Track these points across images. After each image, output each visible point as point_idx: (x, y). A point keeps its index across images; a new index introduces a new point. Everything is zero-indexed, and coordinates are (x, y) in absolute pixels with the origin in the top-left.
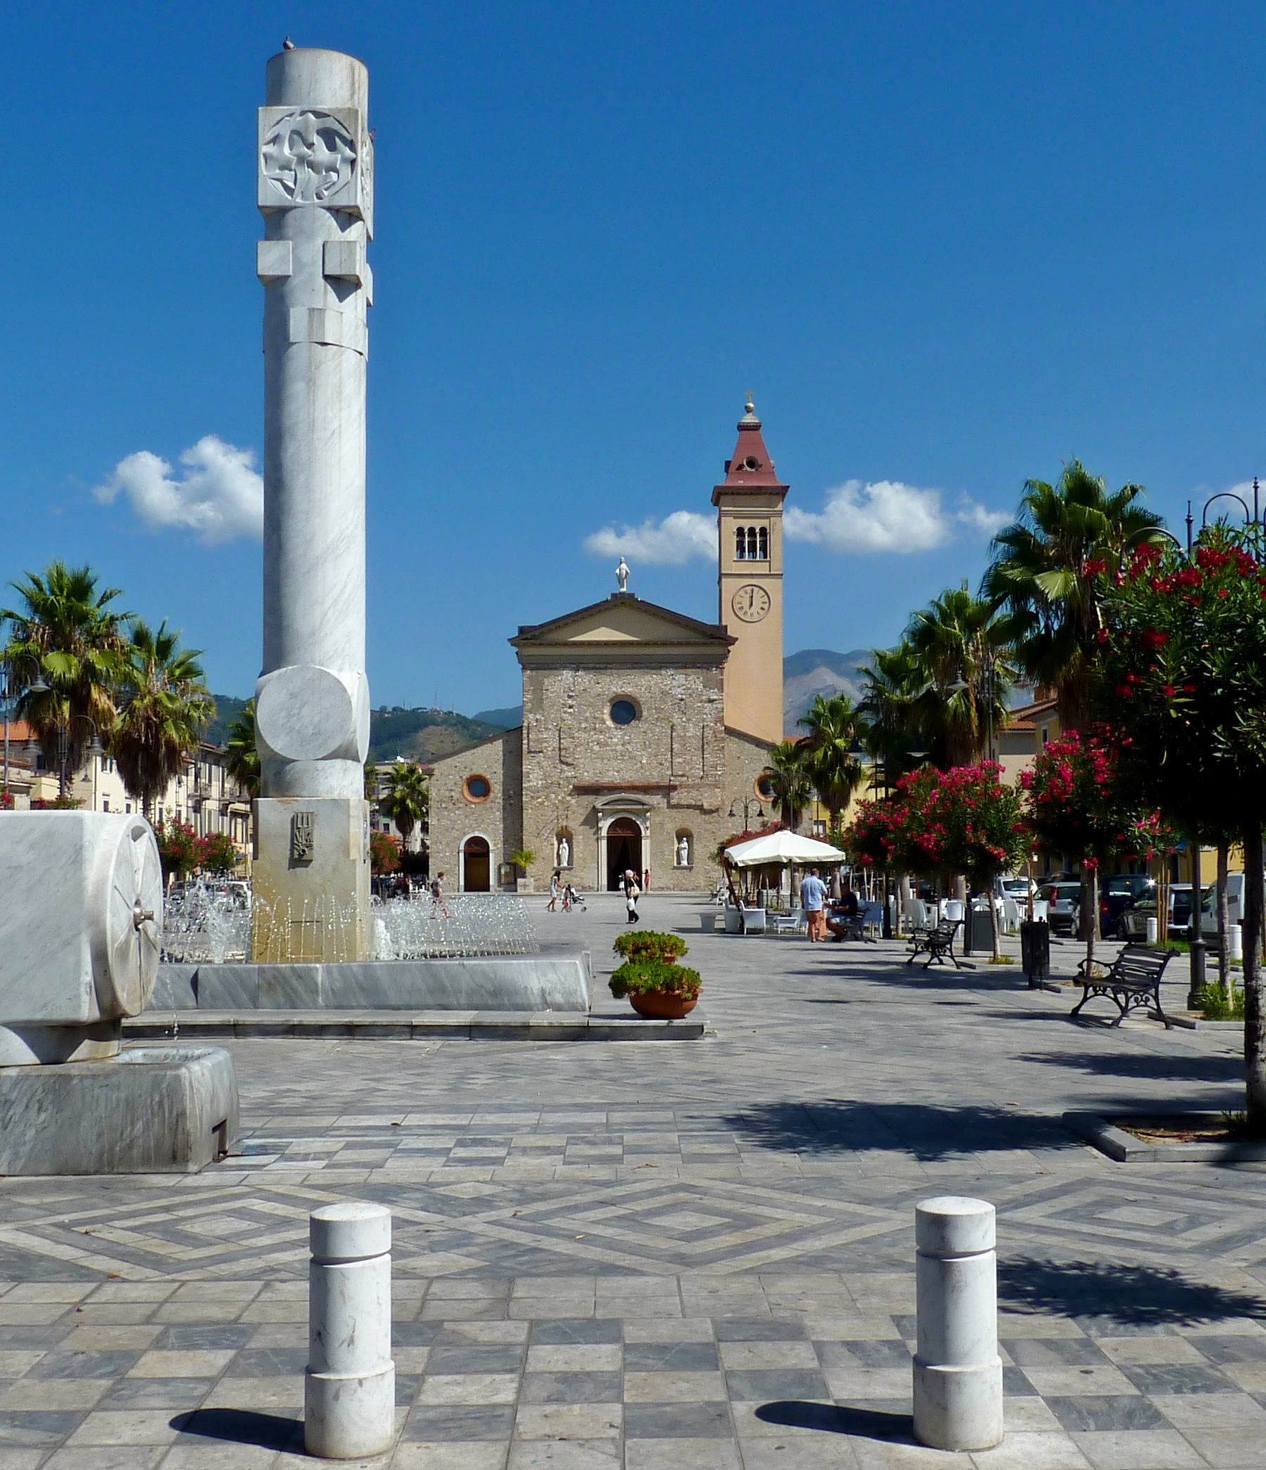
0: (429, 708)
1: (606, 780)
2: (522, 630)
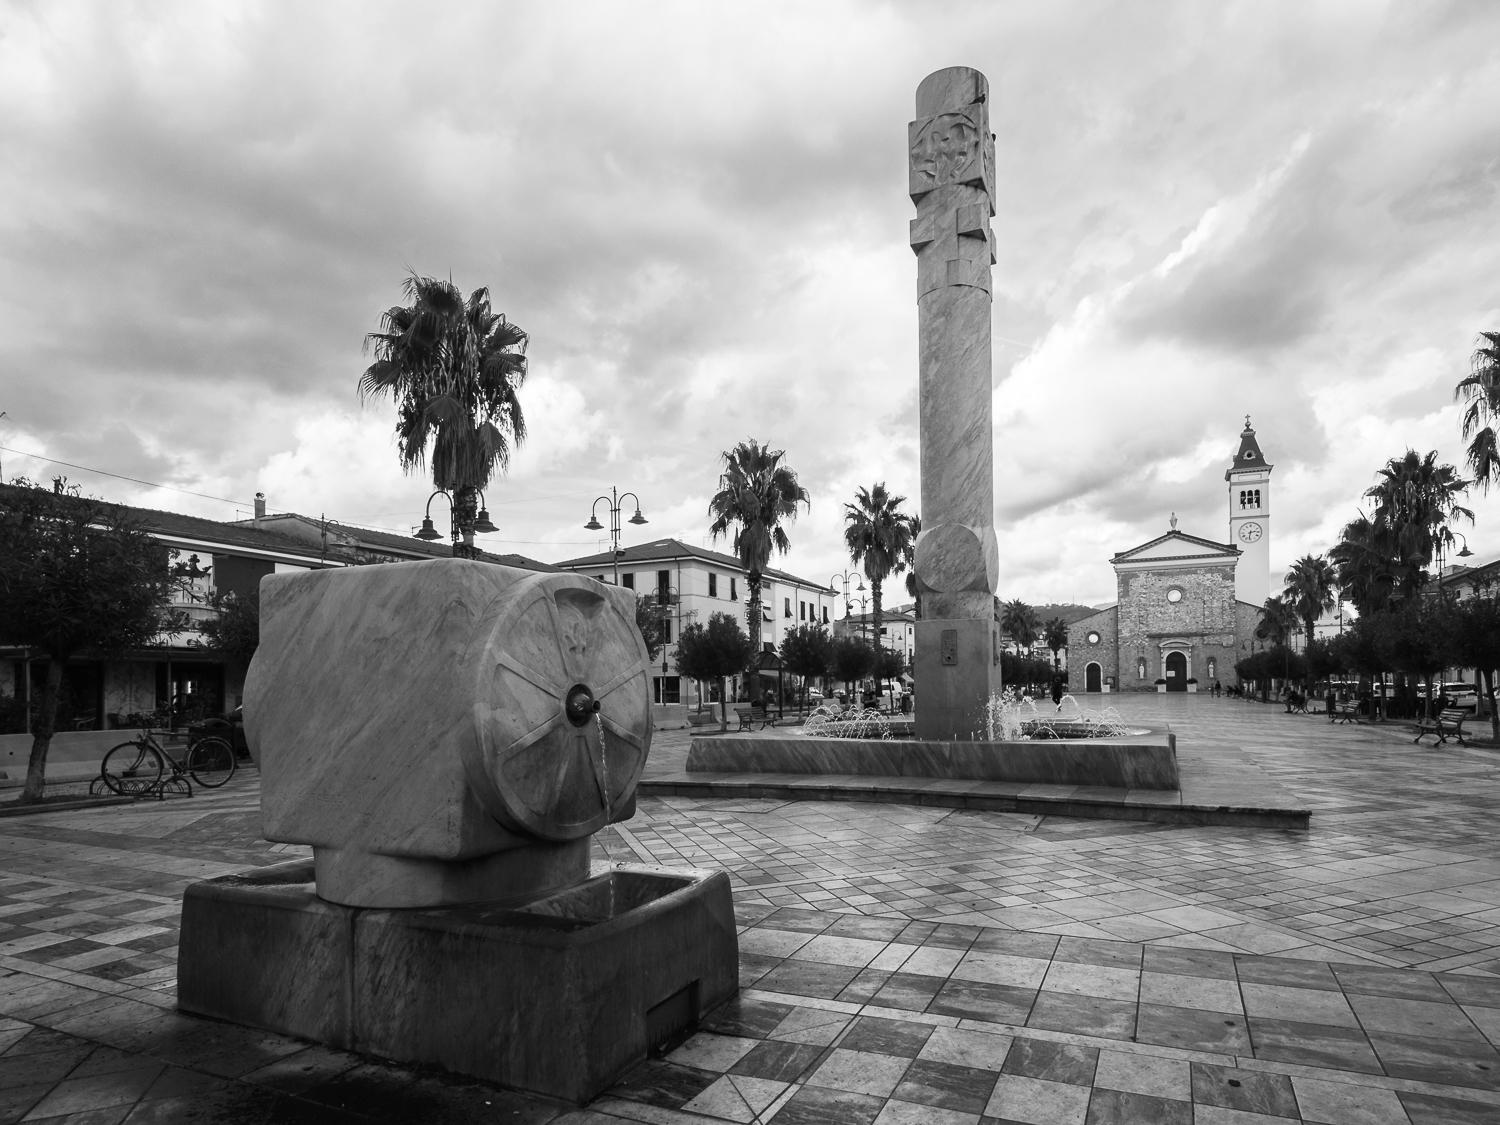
0: (1070, 604)
2: (1117, 555)
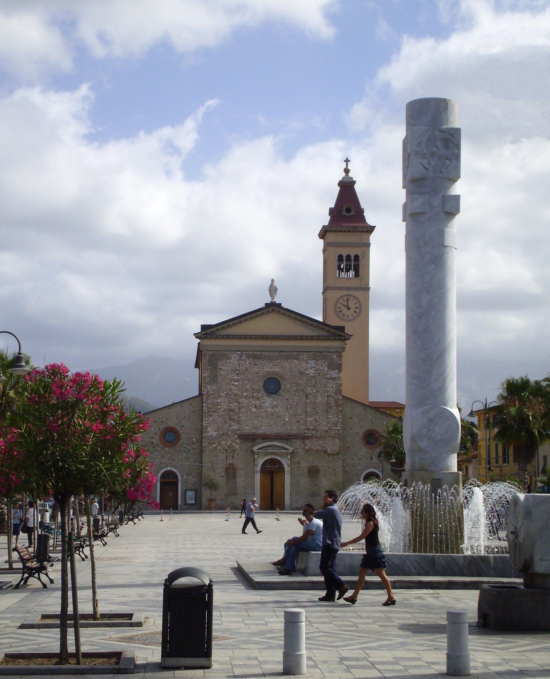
1: (260, 432)
2: (204, 328)
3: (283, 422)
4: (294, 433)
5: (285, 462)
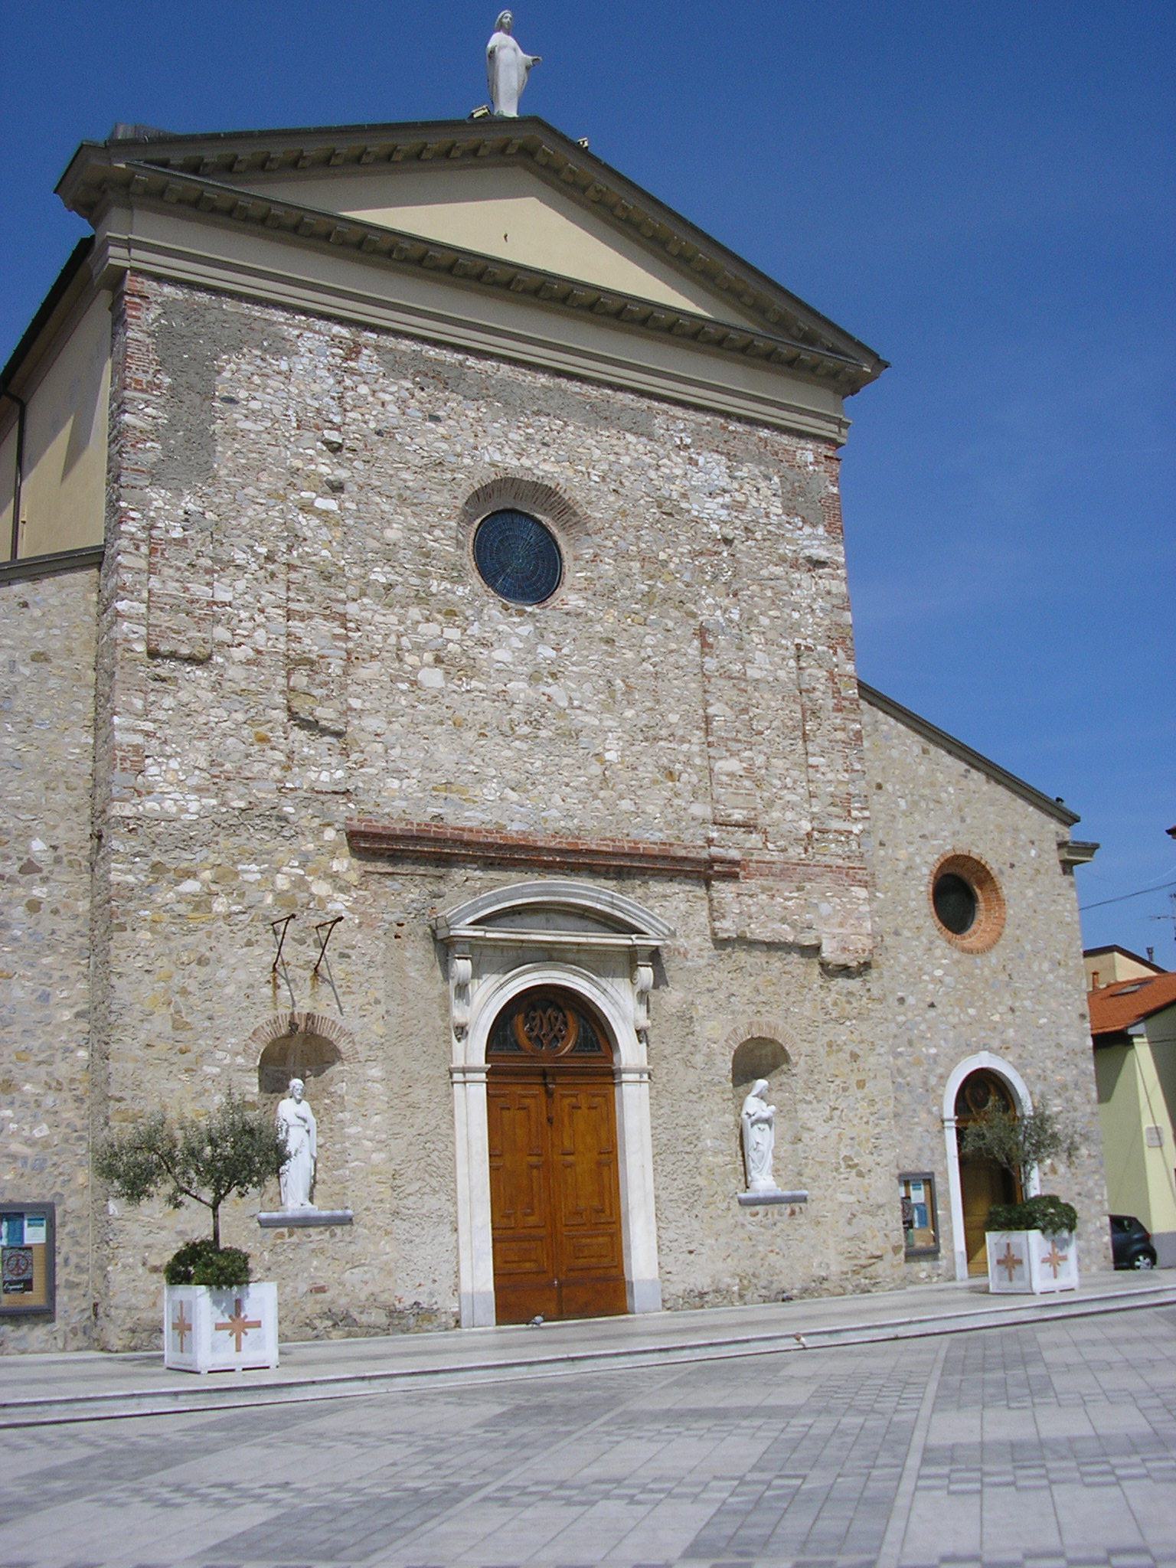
3: (596, 769)
4: (658, 836)
5: (618, 1003)
